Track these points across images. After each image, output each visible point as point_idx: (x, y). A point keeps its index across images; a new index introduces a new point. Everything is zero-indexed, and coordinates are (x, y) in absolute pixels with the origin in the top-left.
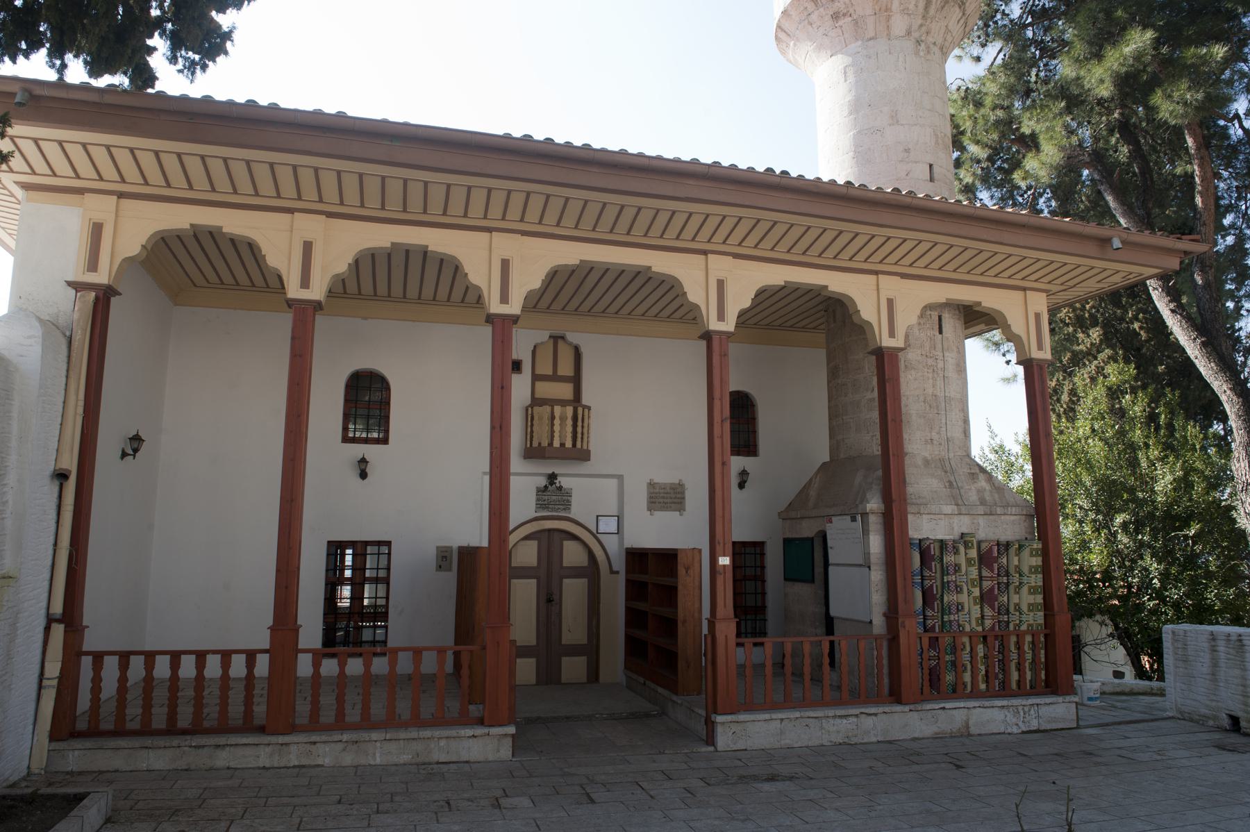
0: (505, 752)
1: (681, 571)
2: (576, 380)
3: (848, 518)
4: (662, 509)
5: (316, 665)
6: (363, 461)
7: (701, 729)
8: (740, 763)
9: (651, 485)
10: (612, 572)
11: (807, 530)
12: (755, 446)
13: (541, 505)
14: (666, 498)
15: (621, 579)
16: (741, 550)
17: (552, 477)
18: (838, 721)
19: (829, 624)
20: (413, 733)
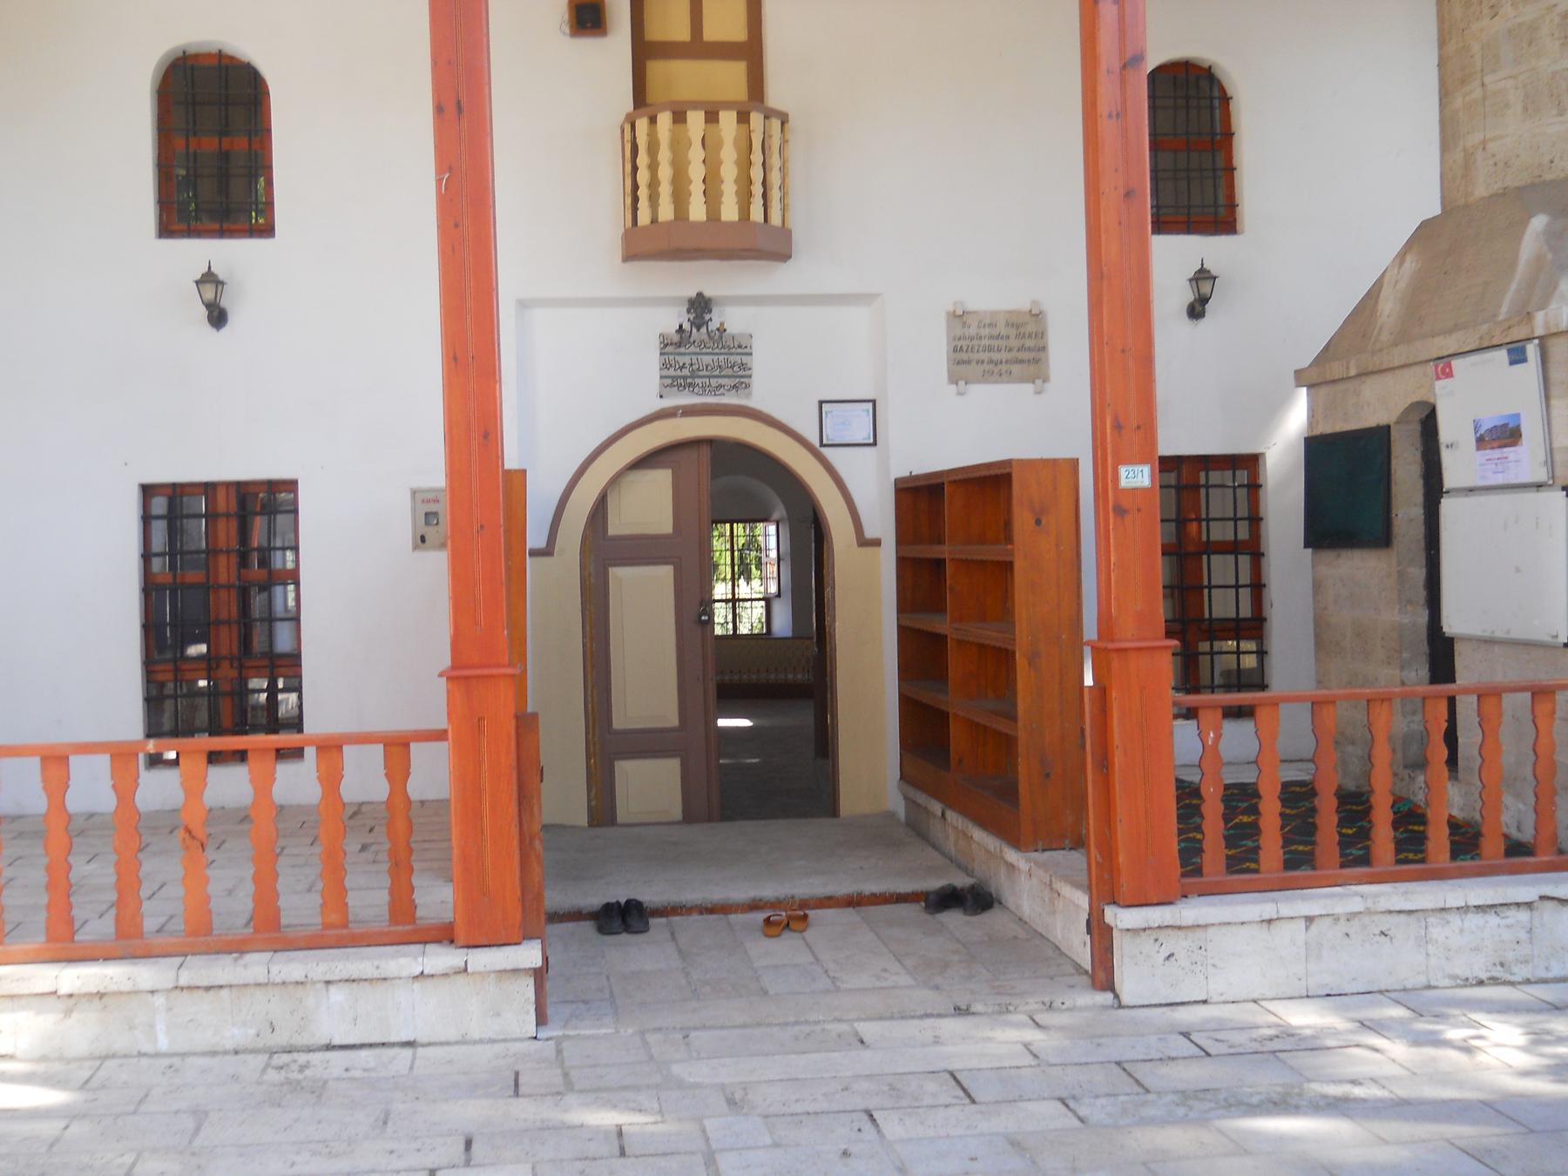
0: (516, 1010)
1: (1022, 519)
2: (751, 52)
3: (1502, 355)
4: (986, 378)
5: (125, 788)
6: (209, 278)
7: (1081, 949)
8: (1186, 1048)
9: (958, 317)
10: (865, 542)
11: (1376, 405)
12: (1232, 206)
13: (675, 379)
14: (997, 349)
15: (886, 561)
16: (1186, 476)
17: (700, 306)
18: (1474, 920)
19: (1441, 655)
20: (255, 966)
